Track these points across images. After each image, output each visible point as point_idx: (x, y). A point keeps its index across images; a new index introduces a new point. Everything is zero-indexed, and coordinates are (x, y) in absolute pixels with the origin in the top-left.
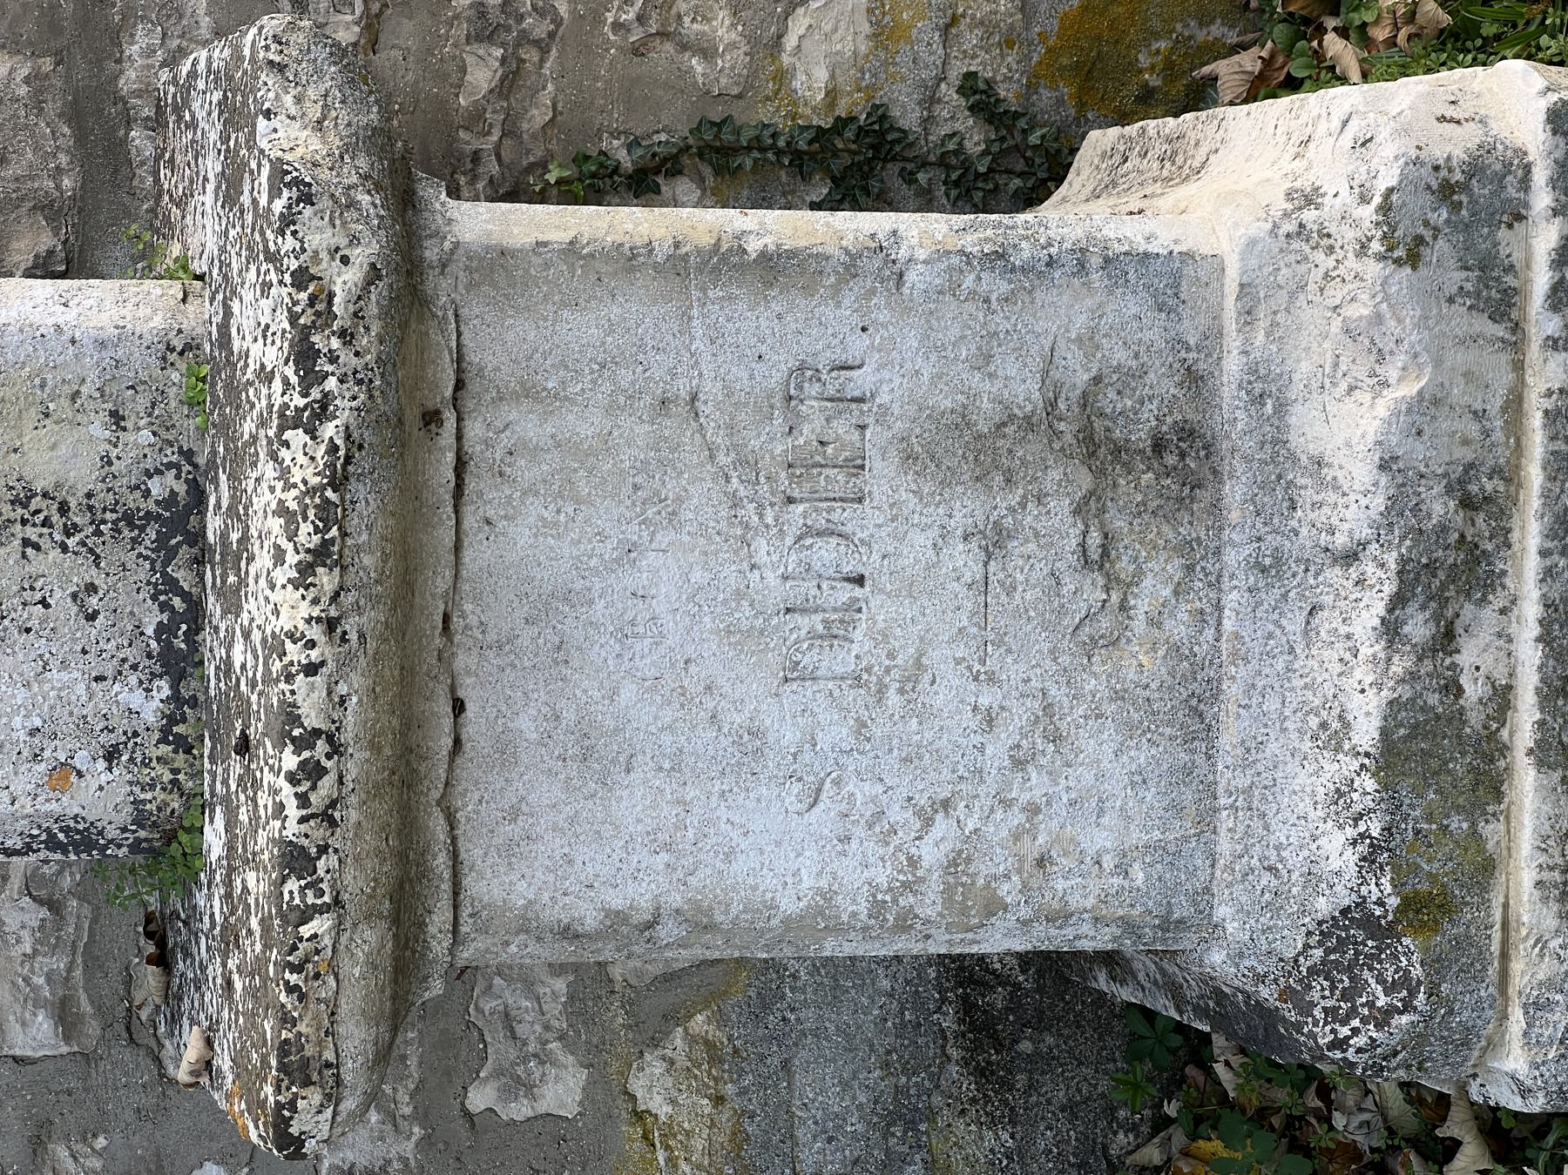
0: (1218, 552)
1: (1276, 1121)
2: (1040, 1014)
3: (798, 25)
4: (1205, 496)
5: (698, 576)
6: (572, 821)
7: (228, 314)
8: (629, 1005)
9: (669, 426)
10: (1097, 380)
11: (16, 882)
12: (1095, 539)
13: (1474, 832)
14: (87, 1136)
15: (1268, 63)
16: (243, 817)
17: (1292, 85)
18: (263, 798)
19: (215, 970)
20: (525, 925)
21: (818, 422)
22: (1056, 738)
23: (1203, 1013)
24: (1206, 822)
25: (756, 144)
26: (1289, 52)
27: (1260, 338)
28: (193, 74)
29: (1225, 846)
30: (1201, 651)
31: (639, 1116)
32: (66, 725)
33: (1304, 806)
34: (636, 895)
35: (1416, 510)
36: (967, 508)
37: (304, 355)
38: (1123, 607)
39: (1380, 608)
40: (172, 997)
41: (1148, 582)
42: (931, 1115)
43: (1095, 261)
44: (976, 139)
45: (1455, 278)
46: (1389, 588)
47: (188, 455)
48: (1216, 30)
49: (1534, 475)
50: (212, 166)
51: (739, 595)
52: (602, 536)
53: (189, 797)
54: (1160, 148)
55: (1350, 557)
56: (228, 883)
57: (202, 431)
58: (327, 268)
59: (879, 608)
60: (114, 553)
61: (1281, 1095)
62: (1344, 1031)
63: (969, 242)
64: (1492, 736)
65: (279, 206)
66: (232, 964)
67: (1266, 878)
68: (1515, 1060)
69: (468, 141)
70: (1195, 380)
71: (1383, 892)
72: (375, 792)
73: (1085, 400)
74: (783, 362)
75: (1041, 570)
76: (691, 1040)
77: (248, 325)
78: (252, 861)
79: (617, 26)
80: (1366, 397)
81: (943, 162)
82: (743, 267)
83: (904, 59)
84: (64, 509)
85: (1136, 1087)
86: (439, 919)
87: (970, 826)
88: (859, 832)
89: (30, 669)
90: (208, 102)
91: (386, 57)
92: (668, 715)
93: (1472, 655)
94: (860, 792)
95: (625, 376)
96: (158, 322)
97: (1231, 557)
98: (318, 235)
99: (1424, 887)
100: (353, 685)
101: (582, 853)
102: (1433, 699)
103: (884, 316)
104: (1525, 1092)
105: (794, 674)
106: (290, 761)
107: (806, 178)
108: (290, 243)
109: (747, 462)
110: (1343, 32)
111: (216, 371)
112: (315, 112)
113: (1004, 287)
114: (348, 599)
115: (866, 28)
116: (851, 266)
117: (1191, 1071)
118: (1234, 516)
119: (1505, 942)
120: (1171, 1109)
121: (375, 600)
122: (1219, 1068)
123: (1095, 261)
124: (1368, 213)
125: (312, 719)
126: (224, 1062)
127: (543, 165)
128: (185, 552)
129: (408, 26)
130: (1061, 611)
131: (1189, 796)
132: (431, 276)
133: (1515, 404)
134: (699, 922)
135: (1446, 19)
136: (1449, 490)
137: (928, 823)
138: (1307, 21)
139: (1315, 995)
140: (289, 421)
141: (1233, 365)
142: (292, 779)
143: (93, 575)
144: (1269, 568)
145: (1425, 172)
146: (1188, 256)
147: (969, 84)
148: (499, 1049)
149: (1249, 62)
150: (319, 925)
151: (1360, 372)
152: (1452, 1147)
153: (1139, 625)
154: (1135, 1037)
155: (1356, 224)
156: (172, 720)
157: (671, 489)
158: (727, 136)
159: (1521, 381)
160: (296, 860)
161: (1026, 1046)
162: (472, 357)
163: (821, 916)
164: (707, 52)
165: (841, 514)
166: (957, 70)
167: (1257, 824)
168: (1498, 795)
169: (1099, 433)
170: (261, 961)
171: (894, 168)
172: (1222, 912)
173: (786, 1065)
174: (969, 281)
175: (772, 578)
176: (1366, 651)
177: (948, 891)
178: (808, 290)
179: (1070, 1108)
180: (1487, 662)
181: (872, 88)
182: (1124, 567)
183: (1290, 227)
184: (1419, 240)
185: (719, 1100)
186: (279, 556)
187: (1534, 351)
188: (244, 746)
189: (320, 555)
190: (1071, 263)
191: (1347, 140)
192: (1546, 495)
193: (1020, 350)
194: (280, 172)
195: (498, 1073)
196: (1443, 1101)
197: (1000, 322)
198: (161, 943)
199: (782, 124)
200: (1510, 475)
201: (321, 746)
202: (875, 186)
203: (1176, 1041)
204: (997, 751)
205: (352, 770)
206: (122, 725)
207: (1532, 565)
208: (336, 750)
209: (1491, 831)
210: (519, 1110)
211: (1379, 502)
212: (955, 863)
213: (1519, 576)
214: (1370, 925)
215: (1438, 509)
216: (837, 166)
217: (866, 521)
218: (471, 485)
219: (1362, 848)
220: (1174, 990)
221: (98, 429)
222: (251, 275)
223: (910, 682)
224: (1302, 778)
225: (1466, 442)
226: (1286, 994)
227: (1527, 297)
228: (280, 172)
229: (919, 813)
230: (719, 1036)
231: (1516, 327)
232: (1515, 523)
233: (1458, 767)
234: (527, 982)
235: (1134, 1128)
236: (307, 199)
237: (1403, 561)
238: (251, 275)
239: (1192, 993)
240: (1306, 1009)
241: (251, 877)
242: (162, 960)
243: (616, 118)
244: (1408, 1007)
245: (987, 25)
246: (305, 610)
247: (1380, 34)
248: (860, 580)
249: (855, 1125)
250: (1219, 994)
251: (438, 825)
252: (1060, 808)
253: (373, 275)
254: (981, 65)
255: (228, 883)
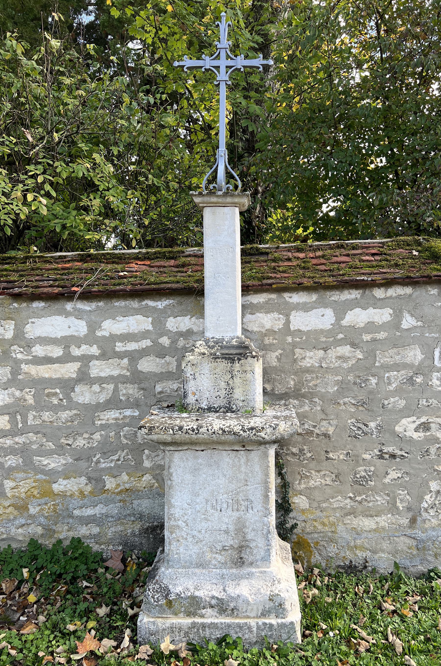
0: (225, 568)
1: (138, 578)
2: (156, 538)
3: (304, 498)
4: (234, 566)
5: (221, 486)
6: (186, 468)
7: (258, 417)
8: (159, 474)
9: (243, 481)
10: (251, 548)
11: (180, 386)
12: (227, 548)
13: (182, 612)
14: (144, 396)
15: (301, 573)
16: (188, 420)
17: (298, 577)
18: (190, 423)
19: (166, 415)
20: (171, 461)
21: (244, 504)
22: (197, 542)
23: (155, 566)
24: (184, 567)
25: (286, 491)
26: (303, 576)
27: (258, 574)
28: (292, 411)
29: (180, 570)
30: (210, 566)
31: (143, 475)
32: (201, 394)
33: (186, 583)
34: (175, 477)
35: (232, 601)
36: (231, 528)
37: (252, 429)
38: (217, 553)
39: (216, 595)
40: (163, 408)
41: (221, 557)
42: (141, 521)
43: (269, 548)
44: (288, 526)
45: (267, 607)
46: (219, 597)
47: (239, 411)
48: (306, 564)
49: (237, 621)
50: (279, 414)
51: (219, 492)
52: (227, 471)
53: (191, 411)
54: (287, 556)
55: (224, 590)
56: (178, 417)
57: (242, 412)
58: (264, 432)
59: (216, 514)
60: (225, 401)
61: (142, 579)
62: (151, 590)
63: (271, 527)
64: (196, 615)
65: (273, 425)
66: (167, 418)
67: (175, 577)
68: (146, 620)
69: (285, 448)
70: (251, 564)
71: (172, 597)
72: (190, 439)
73: (248, 546)
74: (253, 499)
75: (222, 540)
76: (154, 483)
77: (256, 420)
78: (181, 421)
79: (302, 470)
80: (249, 592)
81: (285, 520)
82: (266, 492)
83: (300, 514)
84: (231, 394)
85: (144, 554)
86: (172, 448)
87: (184, 529)
88: (183, 511)
89: (209, 389)
90: (287, 413)
91: (296, 436)
92: (201, 482)
93: (209, 611)
94: (190, 512)
95: (250, 475)
96: (257, 406)
97: (224, 570)
98: (269, 431)
99: (173, 604)
100: (205, 436)
101: (181, 469)
102: (202, 605)
103: (260, 514)
104: (141, 621)
105: (207, 501)
106: (195, 427)
107: (281, 499)
108: (268, 426)
109: (238, 493)
110: (306, 585)
111: (250, 415)
112: (286, 430)
113: (265, 533)
114: (218, 435)
115: (304, 508)
116: (267, 509)
117: (146, 563)
118: (231, 571)
119: (164, 617)
120: (141, 560)
121: (217, 439)
122: (147, 568)
123: (269, 548)
124: (277, 592)
125: (200, 430)
126: (153, 417)
127: (282, 459)
128: (225, 410)
129: (301, 439)
130: (216, 543)
131: (188, 564)
132: (264, 446)
133: (248, 617)
134: (170, 487)
135: (308, 603)
136: (235, 606)
137: (185, 522)
138: (307, 579)
139: (157, 585)
140: (243, 426)
141: (254, 570)
142: (192, 428)
143: (222, 398)
144: (223, 577)
145: (283, 601)
146: (270, 562)
147: (296, 524)
148: (154, 454)
149: (301, 570)
150: (171, 432)
151: (253, 591)
152: (133, 609)
153: (214, 555)
154: (152, 554)
155: (275, 590)
156: (201, 409)
157: (234, 482)
158: (287, 487)
159: (252, 618)
160: (181, 428)
161: (151, 536)
162: (253, 452)
163: (171, 506)
164: (299, 484)
165: (230, 508)
166: (298, 523)
167: (183, 576)
168: (187, 616)
169: (243, 548)
170: (166, 423)
171: (283, 513)
172: (170, 570)
173: (150, 498)
174: (265, 527)
175: (221, 497)
176: (210, 593)
177: (174, 526)
178: (263, 502)
179: (141, 543)
180: (208, 614)
181: (295, 509)
182: (223, 553)
183: (275, 579)
184: (273, 601)
185: (145, 488)
186: (224, 425)
187: (256, 620)
188: (197, 420)
189: (224, 431)
190: (268, 544)
191: (288, 588)
192: (234, 623)
193: (255, 536)
194: (277, 425)
195: (150, 454)
196: (139, 607)
197: (259, 532)
198: (170, 406)
199: (289, 495)
200: (237, 617)
201: (197, 432)
202: (281, 510)
203: (151, 561)
204: (195, 533)
205: (193, 436)
206: (201, 402)
207: (223, 621)
208: (196, 434)
209: (181, 615)
210: (144, 457)
211: (233, 595)
212: (178, 526)
213: (221, 619)
214: (167, 595)
215: (232, 605)
216: (283, 504)
217: (230, 512)
218: (234, 452)
219: (179, 593)
220: (158, 562)
221: (242, 398)
222: (263, 420)
223: (206, 519)
224: (190, 583)
225: (242, 609)
226: (157, 581)
227: (265, 619)
228: (277, 425)
229: (186, 521)
230: (154, 488)
231: (260, 617)
232: (230, 618)
233: (192, 609)
234: (163, 458)
235: (138, 554)
236: (274, 429)
237: (224, 599)
238: (263, 420)
239: (158, 564)
240: (155, 584)
241: (179, 421)
242: (168, 407)
243: (289, 470)
244: (155, 601)
245: (305, 527)
246: (216, 429)
247: (305, 592)
248: (221, 511)
249: (140, 509)
250: (157, 569)
251: (186, 448)
252: (186, 543)
253: (264, 438)
254: (299, 527)
255: (178, 417)
